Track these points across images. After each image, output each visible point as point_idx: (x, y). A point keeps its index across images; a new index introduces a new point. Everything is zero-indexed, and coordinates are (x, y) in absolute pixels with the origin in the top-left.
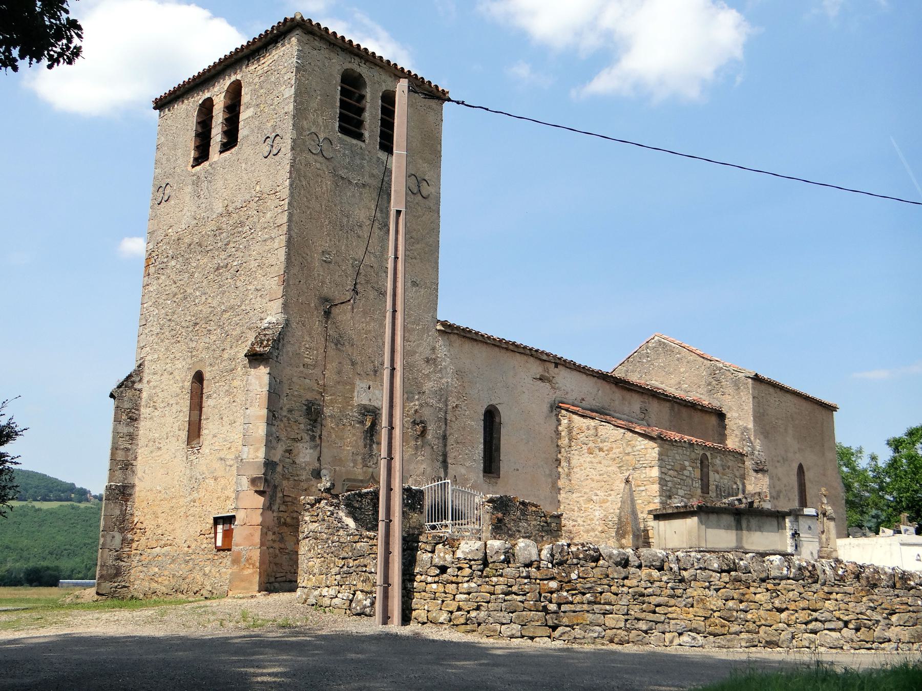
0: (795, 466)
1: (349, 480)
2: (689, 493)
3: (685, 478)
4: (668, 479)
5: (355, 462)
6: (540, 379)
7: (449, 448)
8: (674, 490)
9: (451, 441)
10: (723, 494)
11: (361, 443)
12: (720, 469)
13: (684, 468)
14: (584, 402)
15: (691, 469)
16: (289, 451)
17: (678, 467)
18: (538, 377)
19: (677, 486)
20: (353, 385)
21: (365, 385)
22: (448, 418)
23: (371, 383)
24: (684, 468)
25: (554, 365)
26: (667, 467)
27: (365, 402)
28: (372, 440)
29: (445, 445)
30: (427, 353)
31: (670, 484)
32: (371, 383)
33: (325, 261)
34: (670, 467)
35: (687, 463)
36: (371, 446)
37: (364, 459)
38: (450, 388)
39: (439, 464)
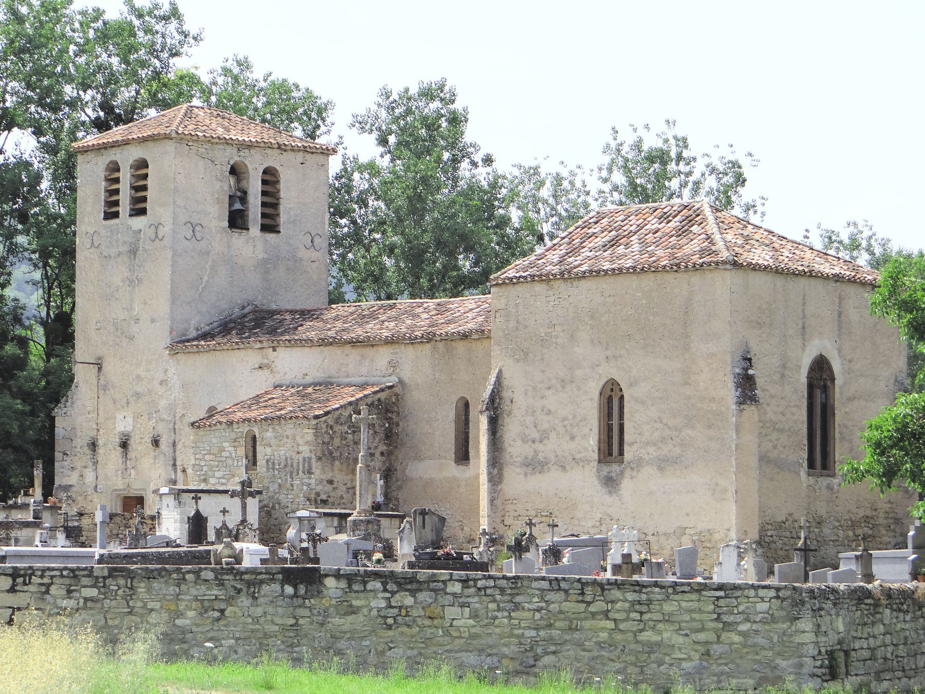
0: (594, 388)
1: (116, 490)
2: (228, 473)
3: (223, 459)
4: (203, 463)
5: (117, 476)
6: (260, 368)
7: (178, 453)
8: (210, 473)
9: (179, 446)
10: (277, 467)
11: (120, 461)
12: (273, 441)
13: (222, 450)
14: (307, 377)
15: (231, 449)
16: (81, 476)
17: (215, 450)
18: (257, 366)
19: (214, 469)
20: (115, 418)
21: (121, 417)
22: (176, 427)
23: (125, 414)
24: (222, 450)
25: (271, 349)
26: (202, 452)
27: (122, 429)
28: (126, 457)
29: (175, 452)
30: (161, 376)
31: (205, 469)
32: (125, 414)
33: (97, 329)
34: (205, 452)
35: (226, 444)
36: (126, 462)
37: (122, 473)
38: (177, 402)
39: (170, 468)
